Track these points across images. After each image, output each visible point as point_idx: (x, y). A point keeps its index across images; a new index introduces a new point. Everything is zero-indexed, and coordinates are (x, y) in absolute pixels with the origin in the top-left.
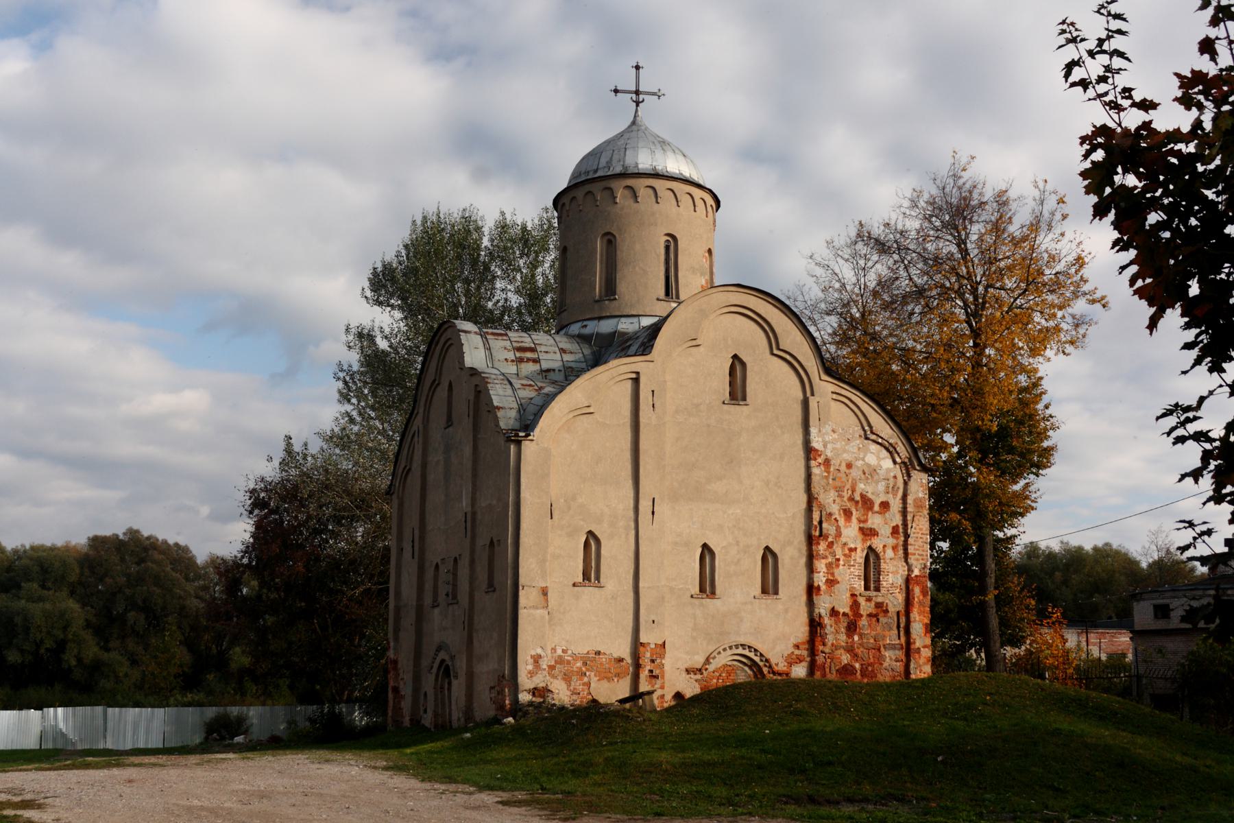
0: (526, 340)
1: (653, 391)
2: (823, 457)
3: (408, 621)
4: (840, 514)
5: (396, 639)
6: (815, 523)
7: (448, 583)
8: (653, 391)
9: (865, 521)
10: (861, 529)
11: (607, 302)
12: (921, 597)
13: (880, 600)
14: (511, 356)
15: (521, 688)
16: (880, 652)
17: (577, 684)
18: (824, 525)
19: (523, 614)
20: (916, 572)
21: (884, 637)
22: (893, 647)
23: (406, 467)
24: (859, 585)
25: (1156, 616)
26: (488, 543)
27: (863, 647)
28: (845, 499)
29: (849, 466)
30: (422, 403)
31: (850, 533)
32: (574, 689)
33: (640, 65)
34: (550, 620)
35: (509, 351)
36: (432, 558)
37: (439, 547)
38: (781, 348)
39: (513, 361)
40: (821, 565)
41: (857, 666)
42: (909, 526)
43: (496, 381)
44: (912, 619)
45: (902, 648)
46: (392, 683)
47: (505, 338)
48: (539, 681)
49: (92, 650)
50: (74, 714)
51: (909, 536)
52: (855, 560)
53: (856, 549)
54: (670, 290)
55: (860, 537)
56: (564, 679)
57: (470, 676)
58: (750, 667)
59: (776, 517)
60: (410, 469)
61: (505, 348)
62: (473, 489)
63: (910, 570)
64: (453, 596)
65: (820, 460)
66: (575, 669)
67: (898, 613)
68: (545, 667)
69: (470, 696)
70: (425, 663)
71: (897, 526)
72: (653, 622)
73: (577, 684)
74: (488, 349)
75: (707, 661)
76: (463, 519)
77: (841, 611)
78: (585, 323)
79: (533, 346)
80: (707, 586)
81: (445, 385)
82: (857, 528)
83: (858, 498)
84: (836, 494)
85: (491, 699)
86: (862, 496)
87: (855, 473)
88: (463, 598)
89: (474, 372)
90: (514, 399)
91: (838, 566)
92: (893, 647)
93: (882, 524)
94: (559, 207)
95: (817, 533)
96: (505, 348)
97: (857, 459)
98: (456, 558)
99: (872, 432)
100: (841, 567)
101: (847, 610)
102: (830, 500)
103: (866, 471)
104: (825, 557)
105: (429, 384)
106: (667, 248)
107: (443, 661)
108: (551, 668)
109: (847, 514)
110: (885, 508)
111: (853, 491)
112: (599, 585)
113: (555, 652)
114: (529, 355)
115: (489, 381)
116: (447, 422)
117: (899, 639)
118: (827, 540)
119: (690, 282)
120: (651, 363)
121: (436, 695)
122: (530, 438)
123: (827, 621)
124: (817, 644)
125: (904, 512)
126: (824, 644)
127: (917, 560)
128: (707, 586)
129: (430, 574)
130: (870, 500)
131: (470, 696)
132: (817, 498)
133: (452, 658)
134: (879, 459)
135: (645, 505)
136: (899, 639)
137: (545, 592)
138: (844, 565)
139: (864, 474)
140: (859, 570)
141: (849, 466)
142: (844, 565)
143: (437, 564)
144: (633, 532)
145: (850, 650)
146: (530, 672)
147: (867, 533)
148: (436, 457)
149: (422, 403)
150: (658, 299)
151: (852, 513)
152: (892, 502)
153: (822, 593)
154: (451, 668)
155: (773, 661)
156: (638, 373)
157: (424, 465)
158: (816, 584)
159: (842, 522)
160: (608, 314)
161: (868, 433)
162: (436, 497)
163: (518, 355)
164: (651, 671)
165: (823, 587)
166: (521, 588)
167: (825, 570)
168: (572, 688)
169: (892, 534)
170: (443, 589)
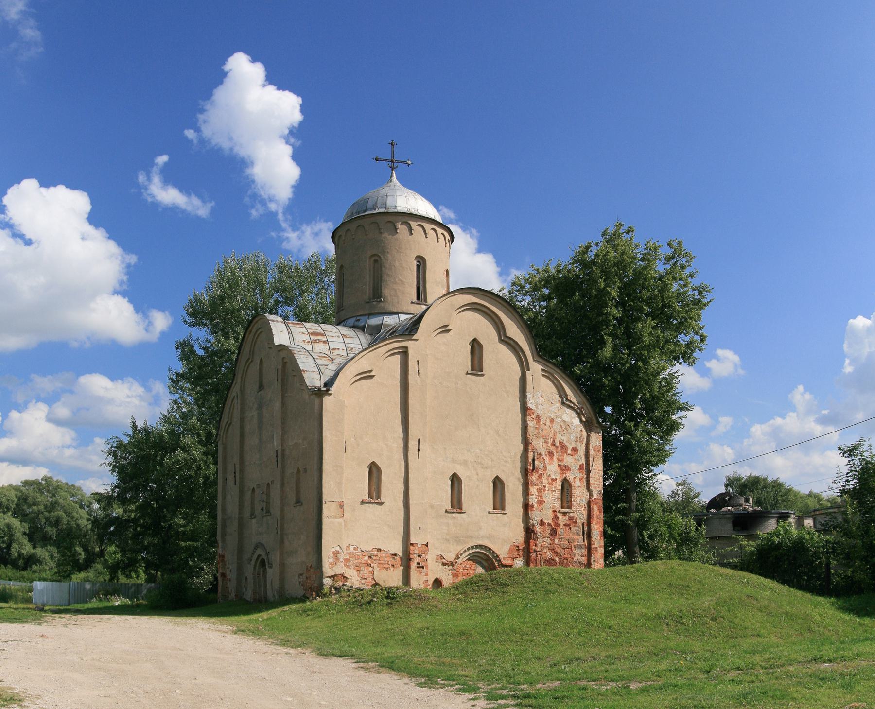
0: (317, 328)
1: (418, 361)
2: (535, 414)
3: (233, 528)
4: (546, 455)
5: (223, 541)
6: (530, 460)
7: (263, 501)
8: (418, 361)
9: (562, 460)
10: (560, 466)
11: (375, 303)
12: (598, 513)
13: (571, 515)
14: (307, 338)
15: (325, 575)
16: (572, 550)
18: (536, 462)
19: (325, 521)
20: (595, 496)
21: (574, 541)
22: (580, 547)
23: (227, 422)
24: (558, 505)
26: (295, 472)
27: (561, 547)
28: (549, 445)
29: (552, 421)
30: (240, 376)
31: (553, 468)
32: (363, 575)
34: (345, 525)
35: (305, 335)
37: (254, 476)
38: (507, 335)
39: (308, 342)
40: (533, 490)
41: (557, 559)
42: (591, 465)
43: (300, 353)
44: (592, 528)
45: (586, 547)
47: (302, 326)
48: (339, 569)
49: (27, 548)
50: (52, 585)
51: (590, 472)
52: (555, 487)
53: (556, 479)
54: (421, 295)
55: (559, 471)
57: (283, 565)
58: (486, 560)
59: (503, 456)
61: (303, 333)
63: (591, 495)
64: (267, 511)
65: (533, 416)
67: (583, 524)
68: (342, 560)
69: (282, 579)
71: (583, 464)
72: (420, 528)
73: (365, 572)
74: (290, 333)
75: (458, 558)
76: (275, 455)
77: (546, 522)
78: (358, 318)
79: (323, 332)
80: (457, 504)
82: (557, 465)
83: (557, 444)
84: (544, 441)
85: (300, 582)
86: (560, 443)
87: (556, 426)
88: (276, 511)
89: (282, 347)
90: (315, 365)
91: (544, 491)
92: (580, 547)
93: (574, 462)
94: (336, 239)
95: (531, 468)
96: (303, 333)
98: (268, 484)
100: (546, 492)
101: (550, 522)
102: (538, 444)
103: (563, 425)
104: (537, 485)
105: (244, 363)
106: (418, 267)
107: (259, 556)
108: (347, 560)
109: (551, 454)
110: (575, 451)
112: (379, 501)
113: (349, 549)
114: (320, 338)
115: (295, 352)
116: (260, 387)
117: (584, 541)
118: (538, 473)
119: (434, 291)
123: (538, 529)
124: (531, 544)
125: (587, 455)
126: (536, 545)
127: (596, 488)
128: (457, 504)
130: (565, 446)
131: (282, 579)
132: (531, 443)
133: (267, 554)
134: (571, 417)
135: (412, 444)
136: (584, 541)
137: (341, 506)
138: (548, 491)
139: (562, 427)
140: (558, 494)
141: (552, 421)
142: (548, 491)
143: (254, 488)
144: (403, 463)
145: (553, 550)
146: (331, 564)
147: (564, 468)
148: (252, 414)
149: (240, 376)
150: (412, 303)
151: (553, 455)
152: (579, 448)
153: (534, 509)
154: (266, 560)
155: (501, 557)
156: (407, 348)
157: (242, 420)
158: (531, 503)
159: (547, 459)
160: (376, 312)
161: (565, 402)
162: (252, 441)
163: (312, 337)
164: (418, 564)
165: (535, 506)
166: (324, 503)
167: (536, 493)
170: (258, 507)
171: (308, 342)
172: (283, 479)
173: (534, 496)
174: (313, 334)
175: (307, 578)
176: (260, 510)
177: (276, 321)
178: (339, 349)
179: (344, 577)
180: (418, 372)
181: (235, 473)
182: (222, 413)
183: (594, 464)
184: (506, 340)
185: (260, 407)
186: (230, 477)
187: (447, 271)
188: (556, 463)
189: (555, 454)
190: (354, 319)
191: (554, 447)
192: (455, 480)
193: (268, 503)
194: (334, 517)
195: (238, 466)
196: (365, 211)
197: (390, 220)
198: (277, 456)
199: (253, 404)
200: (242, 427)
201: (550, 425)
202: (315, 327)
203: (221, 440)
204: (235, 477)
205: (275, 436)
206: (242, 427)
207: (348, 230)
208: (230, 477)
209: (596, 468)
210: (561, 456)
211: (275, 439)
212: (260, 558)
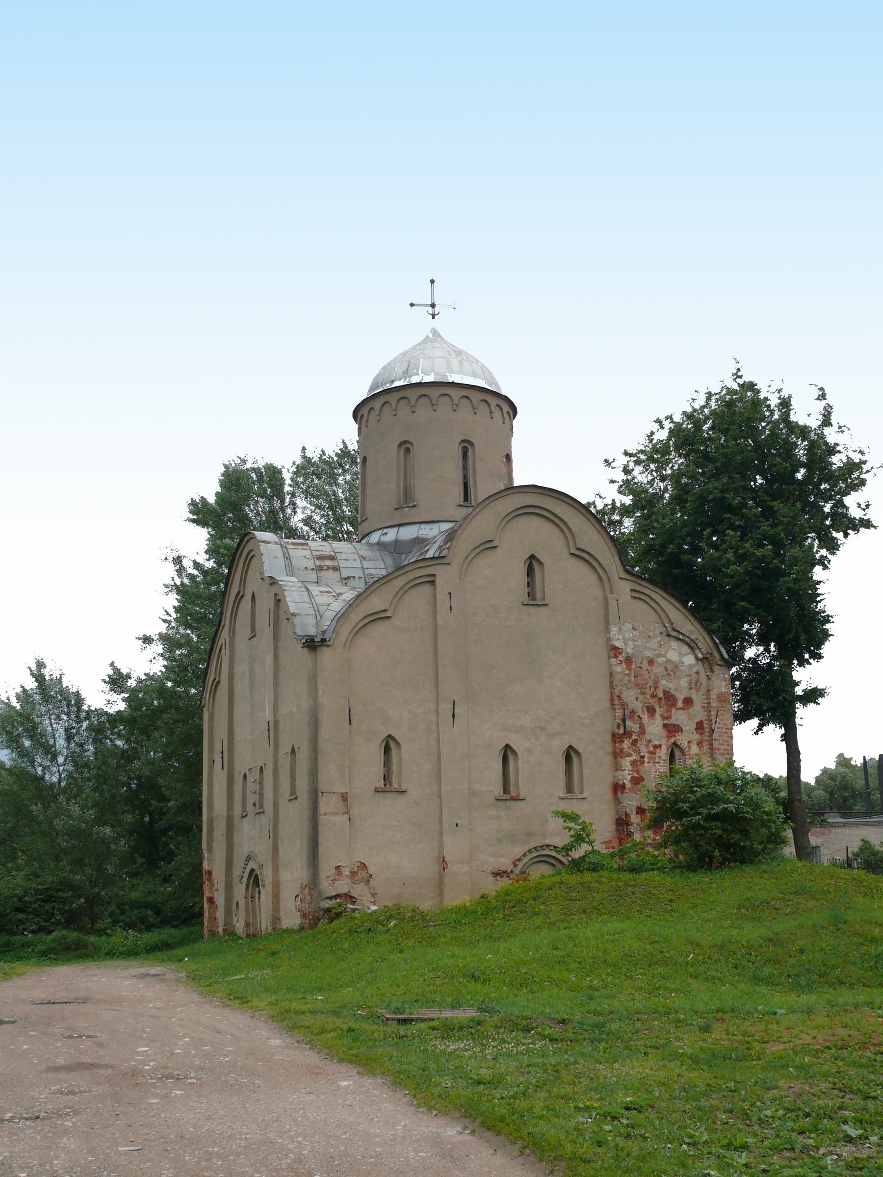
4: (643, 711)
8: (450, 593)
23: (215, 679)
28: (648, 696)
29: (651, 662)
36: (241, 767)
37: (245, 761)
39: (313, 569)
42: (714, 721)
52: (660, 757)
53: (660, 746)
55: (664, 733)
64: (259, 805)
70: (236, 872)
72: (457, 825)
78: (386, 531)
79: (333, 554)
81: (248, 597)
82: (661, 725)
83: (661, 695)
84: (639, 691)
86: (665, 692)
87: (658, 670)
88: (268, 807)
91: (642, 763)
97: (659, 656)
99: (674, 630)
100: (646, 764)
109: (651, 711)
110: (688, 703)
111: (656, 688)
114: (328, 563)
118: (630, 738)
130: (673, 696)
134: (681, 655)
138: (649, 762)
139: (667, 670)
142: (649, 762)
147: (672, 729)
151: (655, 711)
156: (434, 575)
157: (231, 678)
159: (645, 717)
161: (673, 634)
163: (318, 563)
166: (320, 794)
167: (630, 768)
171: (313, 569)
173: (626, 772)
174: (321, 558)
177: (268, 542)
179: (351, 897)
180: (451, 609)
181: (222, 753)
183: (718, 720)
184: (577, 553)
186: (218, 758)
188: (658, 721)
189: (657, 710)
190: (380, 532)
191: (656, 699)
192: (507, 752)
194: (336, 814)
195: (225, 743)
196: (393, 382)
197: (423, 393)
201: (649, 668)
202: (323, 548)
203: (207, 706)
204: (222, 758)
205: (267, 701)
207: (372, 408)
208: (218, 758)
209: (722, 725)
210: (667, 711)
212: (254, 874)
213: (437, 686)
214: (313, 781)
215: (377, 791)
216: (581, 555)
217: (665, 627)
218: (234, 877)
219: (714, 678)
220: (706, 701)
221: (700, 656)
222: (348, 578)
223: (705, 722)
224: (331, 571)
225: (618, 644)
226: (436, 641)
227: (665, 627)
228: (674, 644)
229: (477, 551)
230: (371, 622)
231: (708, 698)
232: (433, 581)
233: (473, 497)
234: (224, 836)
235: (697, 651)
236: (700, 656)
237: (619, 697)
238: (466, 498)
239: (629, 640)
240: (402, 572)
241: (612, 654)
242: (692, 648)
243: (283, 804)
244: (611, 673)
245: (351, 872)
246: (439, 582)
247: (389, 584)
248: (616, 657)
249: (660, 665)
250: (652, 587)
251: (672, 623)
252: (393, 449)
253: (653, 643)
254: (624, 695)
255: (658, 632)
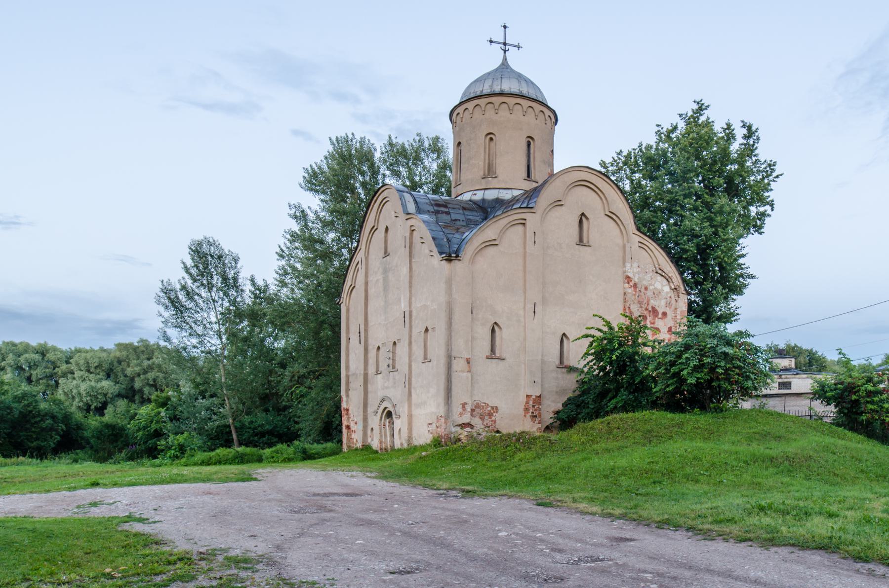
2: (633, 282)
3: (357, 385)
5: (347, 396)
17: (487, 421)
23: (351, 285)
25: (790, 383)
28: (644, 309)
29: (646, 289)
32: (487, 424)
33: (507, 25)
36: (373, 344)
37: (379, 335)
39: (433, 212)
46: (345, 423)
56: (481, 418)
57: (410, 416)
60: (354, 287)
62: (410, 295)
64: (393, 367)
66: (487, 412)
68: (469, 410)
70: (370, 410)
72: (535, 382)
78: (475, 192)
81: (382, 229)
83: (650, 309)
85: (429, 431)
86: (653, 308)
87: (649, 293)
97: (651, 285)
107: (385, 408)
111: (648, 304)
120: (534, 214)
121: (381, 430)
122: (459, 258)
129: (372, 353)
130: (656, 310)
133: (394, 406)
134: (663, 286)
139: (654, 294)
154: (393, 413)
156: (525, 220)
157: (366, 283)
161: (661, 273)
163: (436, 208)
164: (532, 413)
168: (485, 423)
169: (668, 331)
172: (410, 337)
175: (437, 427)
176: (386, 366)
178: (459, 220)
182: (346, 277)
185: (386, 271)
187: (296, 133)
189: (648, 318)
193: (394, 360)
194: (463, 371)
198: (404, 317)
199: (379, 269)
200: (366, 291)
204: (360, 336)
205: (402, 298)
206: (366, 291)
207: (467, 109)
211: (402, 301)
213: (525, 292)
214: (448, 349)
215: (487, 358)
216: (612, 216)
217: (655, 267)
218: (369, 412)
219: (679, 300)
220: (674, 315)
221: (673, 287)
222: (456, 220)
223: (673, 328)
224: (445, 215)
225: (630, 275)
226: (525, 263)
227: (655, 267)
228: (659, 278)
229: (551, 207)
230: (485, 246)
231: (675, 313)
232: (524, 224)
233: (533, 175)
234: (362, 386)
235: (671, 284)
236: (673, 287)
237: (629, 308)
238: (529, 175)
239: (636, 273)
240: (506, 215)
241: (626, 281)
242: (668, 282)
243: (417, 367)
244: (625, 293)
245: (471, 409)
246: (528, 223)
247: (498, 222)
248: (628, 283)
249: (651, 290)
250: (650, 241)
251: (659, 265)
252: (481, 139)
253: (648, 277)
254: (632, 307)
255: (651, 270)
